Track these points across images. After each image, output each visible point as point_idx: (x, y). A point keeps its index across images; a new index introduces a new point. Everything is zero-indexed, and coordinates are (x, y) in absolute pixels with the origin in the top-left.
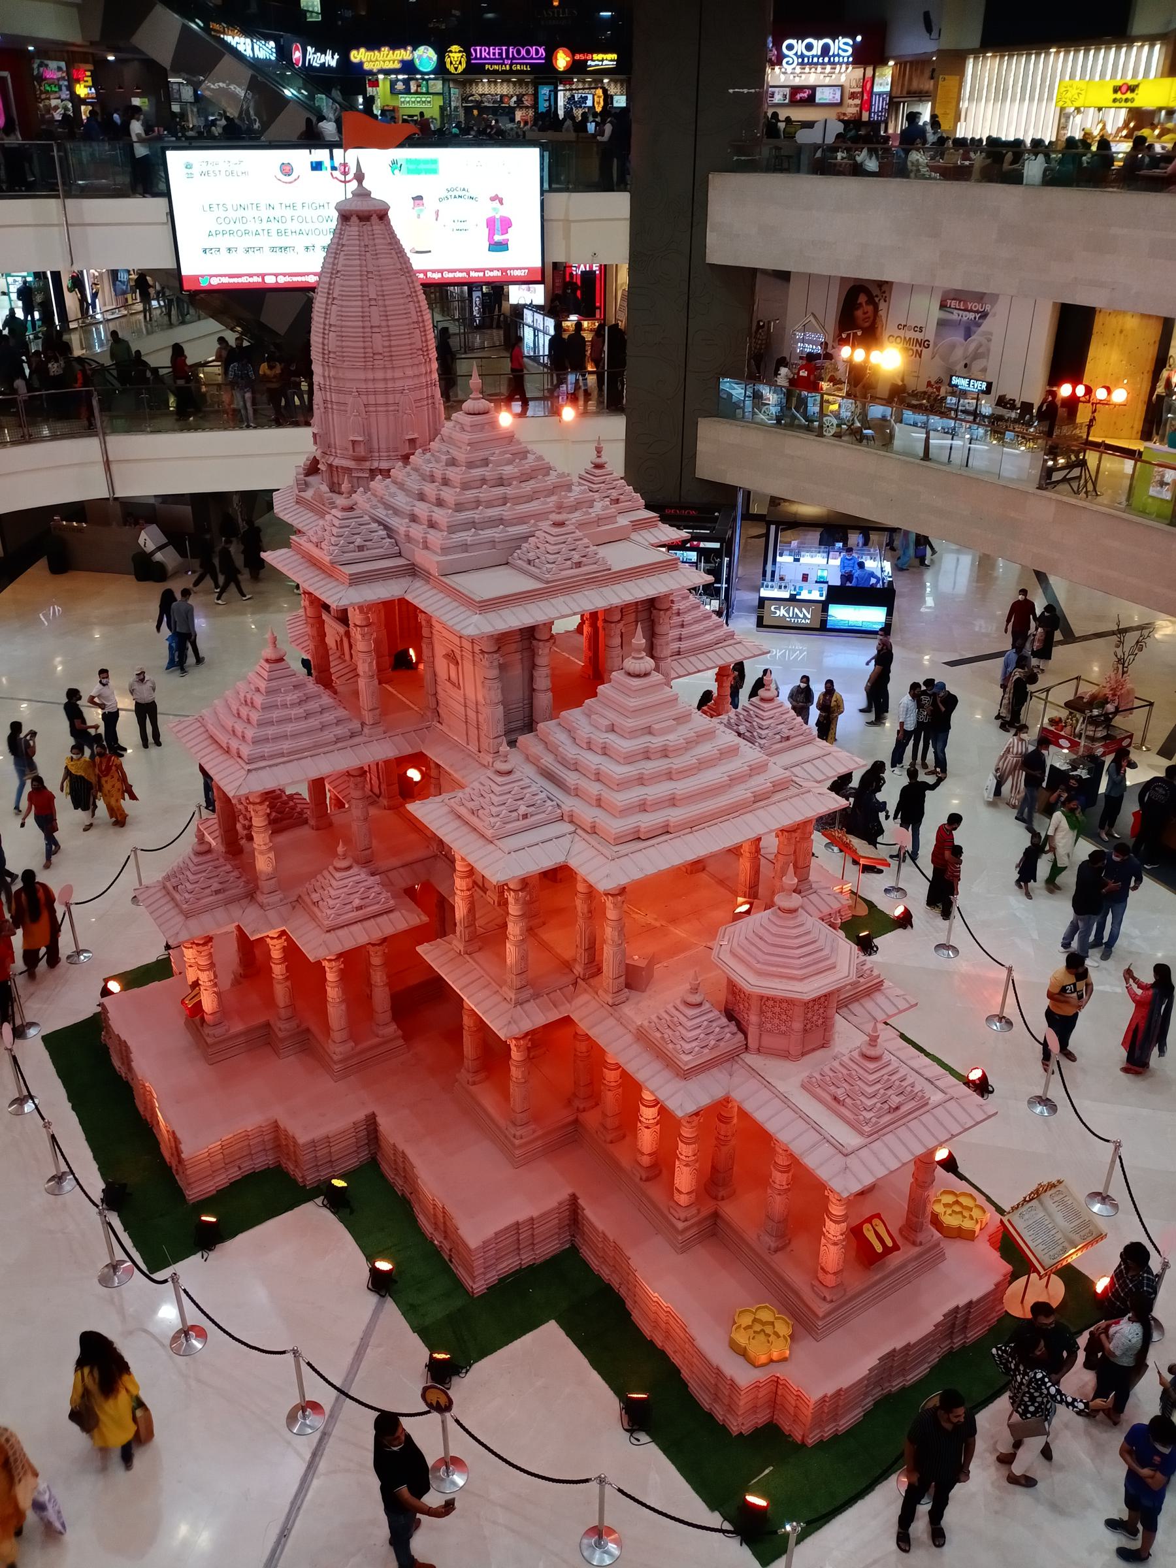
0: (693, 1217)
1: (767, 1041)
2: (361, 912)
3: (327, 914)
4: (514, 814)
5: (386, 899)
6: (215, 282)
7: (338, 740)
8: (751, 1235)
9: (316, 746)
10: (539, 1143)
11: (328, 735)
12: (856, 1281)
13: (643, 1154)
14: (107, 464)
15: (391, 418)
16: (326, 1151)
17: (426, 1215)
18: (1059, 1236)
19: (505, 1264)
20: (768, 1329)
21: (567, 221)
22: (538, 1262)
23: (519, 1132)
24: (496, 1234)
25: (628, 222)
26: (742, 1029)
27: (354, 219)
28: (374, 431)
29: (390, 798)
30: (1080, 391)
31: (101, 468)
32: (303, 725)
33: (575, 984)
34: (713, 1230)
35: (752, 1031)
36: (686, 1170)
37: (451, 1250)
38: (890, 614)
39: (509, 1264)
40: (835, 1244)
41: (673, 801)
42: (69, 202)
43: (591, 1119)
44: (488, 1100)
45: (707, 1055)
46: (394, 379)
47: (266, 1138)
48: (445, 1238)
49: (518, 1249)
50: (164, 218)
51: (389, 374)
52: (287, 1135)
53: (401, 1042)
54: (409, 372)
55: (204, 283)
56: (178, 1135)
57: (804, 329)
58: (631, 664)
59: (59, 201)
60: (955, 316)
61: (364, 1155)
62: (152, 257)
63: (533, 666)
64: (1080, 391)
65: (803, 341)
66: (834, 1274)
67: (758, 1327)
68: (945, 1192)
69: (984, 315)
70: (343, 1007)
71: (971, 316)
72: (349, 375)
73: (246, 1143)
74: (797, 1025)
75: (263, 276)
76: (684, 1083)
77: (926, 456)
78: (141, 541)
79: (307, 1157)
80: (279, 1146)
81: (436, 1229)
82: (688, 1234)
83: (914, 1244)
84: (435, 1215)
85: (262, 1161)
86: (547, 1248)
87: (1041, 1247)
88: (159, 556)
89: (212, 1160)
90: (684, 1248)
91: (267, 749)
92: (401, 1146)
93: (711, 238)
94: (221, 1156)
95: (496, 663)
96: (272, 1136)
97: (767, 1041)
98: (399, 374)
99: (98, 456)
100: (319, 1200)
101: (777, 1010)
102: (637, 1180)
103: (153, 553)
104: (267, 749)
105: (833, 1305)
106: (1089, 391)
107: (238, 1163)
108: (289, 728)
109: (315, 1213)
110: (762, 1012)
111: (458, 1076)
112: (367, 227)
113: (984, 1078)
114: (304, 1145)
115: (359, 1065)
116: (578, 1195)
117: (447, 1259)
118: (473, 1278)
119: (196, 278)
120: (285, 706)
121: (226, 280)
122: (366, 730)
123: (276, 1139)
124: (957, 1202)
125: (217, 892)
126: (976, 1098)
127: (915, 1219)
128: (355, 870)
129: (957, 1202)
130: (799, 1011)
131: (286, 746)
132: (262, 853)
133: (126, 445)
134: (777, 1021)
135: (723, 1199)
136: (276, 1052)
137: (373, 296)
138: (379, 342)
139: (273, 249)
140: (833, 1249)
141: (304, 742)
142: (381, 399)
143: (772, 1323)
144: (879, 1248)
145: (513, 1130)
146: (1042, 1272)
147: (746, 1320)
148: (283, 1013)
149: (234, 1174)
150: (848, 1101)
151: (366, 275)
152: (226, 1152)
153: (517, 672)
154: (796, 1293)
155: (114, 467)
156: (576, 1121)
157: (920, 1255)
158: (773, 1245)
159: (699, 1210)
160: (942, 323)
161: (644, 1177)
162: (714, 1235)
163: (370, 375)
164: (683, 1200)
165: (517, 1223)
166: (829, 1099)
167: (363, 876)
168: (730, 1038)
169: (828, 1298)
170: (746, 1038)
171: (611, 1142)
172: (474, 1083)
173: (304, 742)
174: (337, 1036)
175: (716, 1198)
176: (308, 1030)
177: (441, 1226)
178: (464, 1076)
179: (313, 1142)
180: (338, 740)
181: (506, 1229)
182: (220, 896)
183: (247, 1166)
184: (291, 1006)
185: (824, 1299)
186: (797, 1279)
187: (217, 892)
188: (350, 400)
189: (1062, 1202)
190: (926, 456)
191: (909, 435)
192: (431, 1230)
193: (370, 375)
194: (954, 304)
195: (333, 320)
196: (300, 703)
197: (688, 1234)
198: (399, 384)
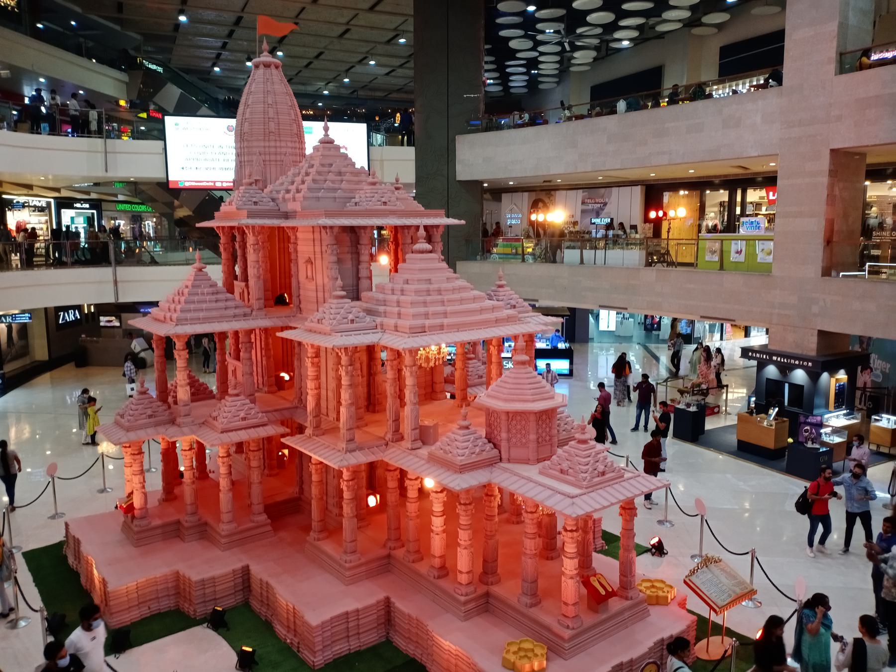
0: (472, 593)
1: (515, 453)
2: (244, 422)
3: (221, 423)
4: (346, 320)
5: (261, 418)
6: (187, 184)
7: (235, 316)
8: (514, 601)
9: (221, 317)
10: (363, 568)
11: (231, 312)
12: (589, 619)
13: (435, 557)
14: (116, 282)
15: (279, 169)
16: (212, 589)
17: (281, 623)
18: (725, 588)
19: (338, 647)
20: (530, 654)
21: (382, 161)
22: (363, 648)
23: (348, 558)
24: (332, 619)
25: (414, 163)
26: (496, 446)
27: (262, 66)
28: (268, 176)
29: (270, 386)
30: (661, 214)
31: (112, 285)
32: (214, 305)
33: (387, 445)
34: (485, 605)
35: (504, 445)
36: (465, 552)
37: (299, 643)
38: (571, 363)
39: (341, 648)
40: (572, 578)
41: (445, 314)
42: (108, 141)
43: (400, 553)
44: (328, 547)
45: (474, 458)
46: (281, 147)
47: (170, 585)
48: (295, 636)
49: (348, 637)
50: (161, 151)
51: (278, 144)
52: (184, 577)
53: (269, 528)
54: (289, 144)
55: (181, 185)
56: (106, 579)
57: (511, 211)
58: (417, 246)
59: (103, 140)
60: (590, 207)
61: (240, 597)
62: (153, 173)
63: (359, 262)
64: (661, 214)
65: (511, 218)
66: (574, 605)
67: (522, 654)
68: (643, 581)
69: (605, 204)
70: (230, 495)
71: (599, 205)
72: (255, 144)
73: (155, 588)
74: (533, 437)
75: (215, 182)
76: (460, 475)
77: (582, 262)
78: (133, 346)
79: (198, 593)
80: (179, 593)
81: (288, 632)
82: (470, 606)
83: (627, 598)
84: (288, 618)
85: (166, 604)
86: (370, 638)
87: (714, 595)
88: (142, 355)
89: (130, 597)
90: (468, 616)
91: (189, 315)
92: (265, 578)
93: (458, 167)
94: (136, 595)
95: (335, 252)
96: (174, 584)
97: (515, 453)
98: (283, 144)
99: (111, 278)
100: (205, 625)
101: (519, 427)
102: (432, 579)
103: (139, 353)
104: (189, 315)
105: (574, 632)
106: (665, 214)
107: (149, 603)
108: (204, 306)
109: (203, 632)
110: (509, 431)
111: (308, 538)
112: (268, 71)
113: (660, 542)
114: (196, 583)
115: (241, 540)
116: (390, 596)
117: (295, 650)
118: (314, 653)
119: (177, 182)
120: (203, 294)
121: (194, 184)
122: (254, 313)
123: (177, 587)
124: (653, 586)
125: (150, 416)
126: (656, 559)
127: (625, 579)
128: (242, 397)
129: (653, 586)
130: (532, 418)
131: (201, 315)
132: (181, 386)
133: (127, 272)
134: (519, 436)
135: (492, 584)
136: (183, 540)
137: (270, 102)
138: (272, 126)
139: (221, 169)
140: (570, 582)
141: (214, 314)
142: (273, 157)
143: (533, 650)
144: (603, 592)
145: (345, 557)
146: (718, 609)
147: (514, 648)
148: (189, 509)
149: (144, 612)
150: (570, 471)
151: (266, 93)
152: (140, 593)
153: (349, 265)
154: (549, 629)
155: (119, 285)
156: (389, 556)
157: (631, 608)
158: (529, 601)
159: (476, 589)
160: (583, 212)
161: (436, 575)
162: (487, 611)
163: (267, 144)
164: (463, 578)
165: (347, 613)
166: (558, 474)
167: (248, 401)
168: (490, 452)
169: (571, 626)
170: (500, 452)
171: (413, 562)
172: (319, 540)
173: (214, 314)
174: (225, 517)
175: (487, 584)
176: (206, 524)
177: (292, 626)
178: (313, 535)
179: (203, 582)
180: (235, 316)
181: (338, 616)
182: (151, 420)
183: (155, 607)
184: (194, 503)
185: (568, 627)
186: (548, 620)
187: (150, 416)
188: (255, 158)
189: (722, 570)
190: (582, 262)
191: (571, 255)
192: (284, 632)
193: (267, 144)
194: (589, 201)
195: (247, 116)
196: (213, 294)
197: (470, 606)
198: (283, 150)
